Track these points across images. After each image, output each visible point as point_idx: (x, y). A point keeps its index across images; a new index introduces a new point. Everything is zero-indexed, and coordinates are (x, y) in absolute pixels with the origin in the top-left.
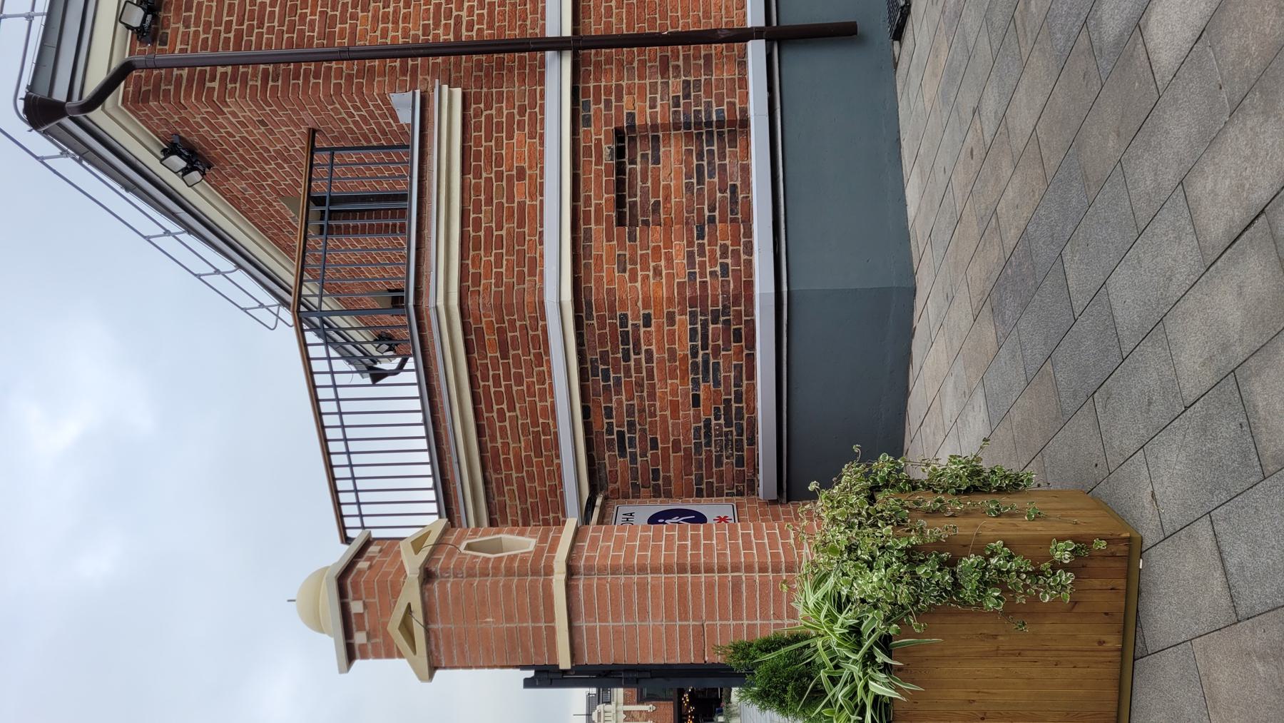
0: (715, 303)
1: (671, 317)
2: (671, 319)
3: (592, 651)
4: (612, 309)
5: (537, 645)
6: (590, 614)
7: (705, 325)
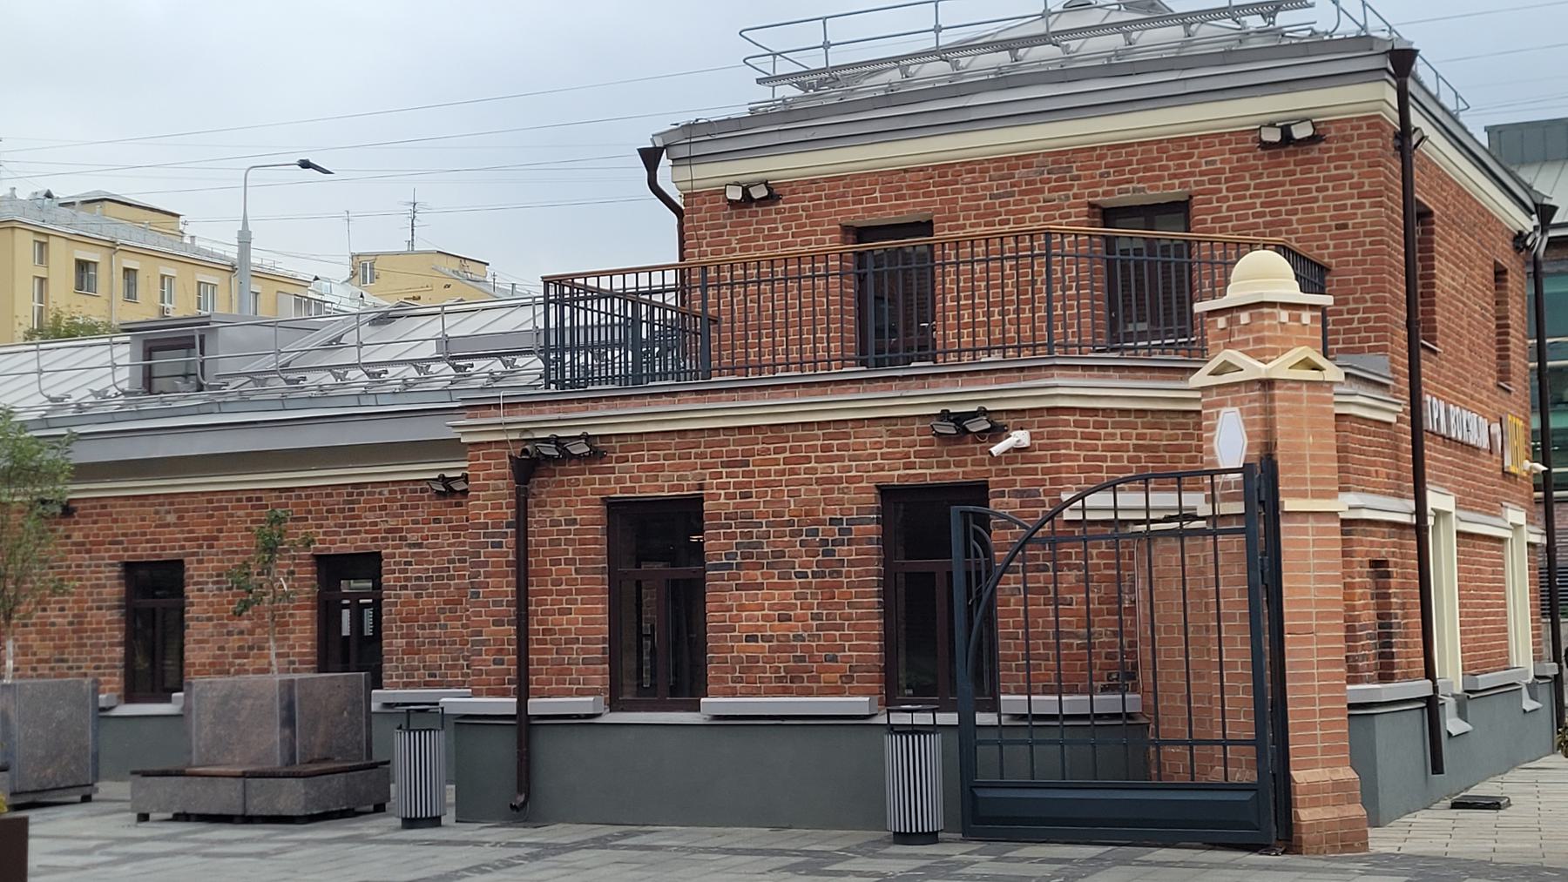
5: (1293, 481)
6: (1319, 531)
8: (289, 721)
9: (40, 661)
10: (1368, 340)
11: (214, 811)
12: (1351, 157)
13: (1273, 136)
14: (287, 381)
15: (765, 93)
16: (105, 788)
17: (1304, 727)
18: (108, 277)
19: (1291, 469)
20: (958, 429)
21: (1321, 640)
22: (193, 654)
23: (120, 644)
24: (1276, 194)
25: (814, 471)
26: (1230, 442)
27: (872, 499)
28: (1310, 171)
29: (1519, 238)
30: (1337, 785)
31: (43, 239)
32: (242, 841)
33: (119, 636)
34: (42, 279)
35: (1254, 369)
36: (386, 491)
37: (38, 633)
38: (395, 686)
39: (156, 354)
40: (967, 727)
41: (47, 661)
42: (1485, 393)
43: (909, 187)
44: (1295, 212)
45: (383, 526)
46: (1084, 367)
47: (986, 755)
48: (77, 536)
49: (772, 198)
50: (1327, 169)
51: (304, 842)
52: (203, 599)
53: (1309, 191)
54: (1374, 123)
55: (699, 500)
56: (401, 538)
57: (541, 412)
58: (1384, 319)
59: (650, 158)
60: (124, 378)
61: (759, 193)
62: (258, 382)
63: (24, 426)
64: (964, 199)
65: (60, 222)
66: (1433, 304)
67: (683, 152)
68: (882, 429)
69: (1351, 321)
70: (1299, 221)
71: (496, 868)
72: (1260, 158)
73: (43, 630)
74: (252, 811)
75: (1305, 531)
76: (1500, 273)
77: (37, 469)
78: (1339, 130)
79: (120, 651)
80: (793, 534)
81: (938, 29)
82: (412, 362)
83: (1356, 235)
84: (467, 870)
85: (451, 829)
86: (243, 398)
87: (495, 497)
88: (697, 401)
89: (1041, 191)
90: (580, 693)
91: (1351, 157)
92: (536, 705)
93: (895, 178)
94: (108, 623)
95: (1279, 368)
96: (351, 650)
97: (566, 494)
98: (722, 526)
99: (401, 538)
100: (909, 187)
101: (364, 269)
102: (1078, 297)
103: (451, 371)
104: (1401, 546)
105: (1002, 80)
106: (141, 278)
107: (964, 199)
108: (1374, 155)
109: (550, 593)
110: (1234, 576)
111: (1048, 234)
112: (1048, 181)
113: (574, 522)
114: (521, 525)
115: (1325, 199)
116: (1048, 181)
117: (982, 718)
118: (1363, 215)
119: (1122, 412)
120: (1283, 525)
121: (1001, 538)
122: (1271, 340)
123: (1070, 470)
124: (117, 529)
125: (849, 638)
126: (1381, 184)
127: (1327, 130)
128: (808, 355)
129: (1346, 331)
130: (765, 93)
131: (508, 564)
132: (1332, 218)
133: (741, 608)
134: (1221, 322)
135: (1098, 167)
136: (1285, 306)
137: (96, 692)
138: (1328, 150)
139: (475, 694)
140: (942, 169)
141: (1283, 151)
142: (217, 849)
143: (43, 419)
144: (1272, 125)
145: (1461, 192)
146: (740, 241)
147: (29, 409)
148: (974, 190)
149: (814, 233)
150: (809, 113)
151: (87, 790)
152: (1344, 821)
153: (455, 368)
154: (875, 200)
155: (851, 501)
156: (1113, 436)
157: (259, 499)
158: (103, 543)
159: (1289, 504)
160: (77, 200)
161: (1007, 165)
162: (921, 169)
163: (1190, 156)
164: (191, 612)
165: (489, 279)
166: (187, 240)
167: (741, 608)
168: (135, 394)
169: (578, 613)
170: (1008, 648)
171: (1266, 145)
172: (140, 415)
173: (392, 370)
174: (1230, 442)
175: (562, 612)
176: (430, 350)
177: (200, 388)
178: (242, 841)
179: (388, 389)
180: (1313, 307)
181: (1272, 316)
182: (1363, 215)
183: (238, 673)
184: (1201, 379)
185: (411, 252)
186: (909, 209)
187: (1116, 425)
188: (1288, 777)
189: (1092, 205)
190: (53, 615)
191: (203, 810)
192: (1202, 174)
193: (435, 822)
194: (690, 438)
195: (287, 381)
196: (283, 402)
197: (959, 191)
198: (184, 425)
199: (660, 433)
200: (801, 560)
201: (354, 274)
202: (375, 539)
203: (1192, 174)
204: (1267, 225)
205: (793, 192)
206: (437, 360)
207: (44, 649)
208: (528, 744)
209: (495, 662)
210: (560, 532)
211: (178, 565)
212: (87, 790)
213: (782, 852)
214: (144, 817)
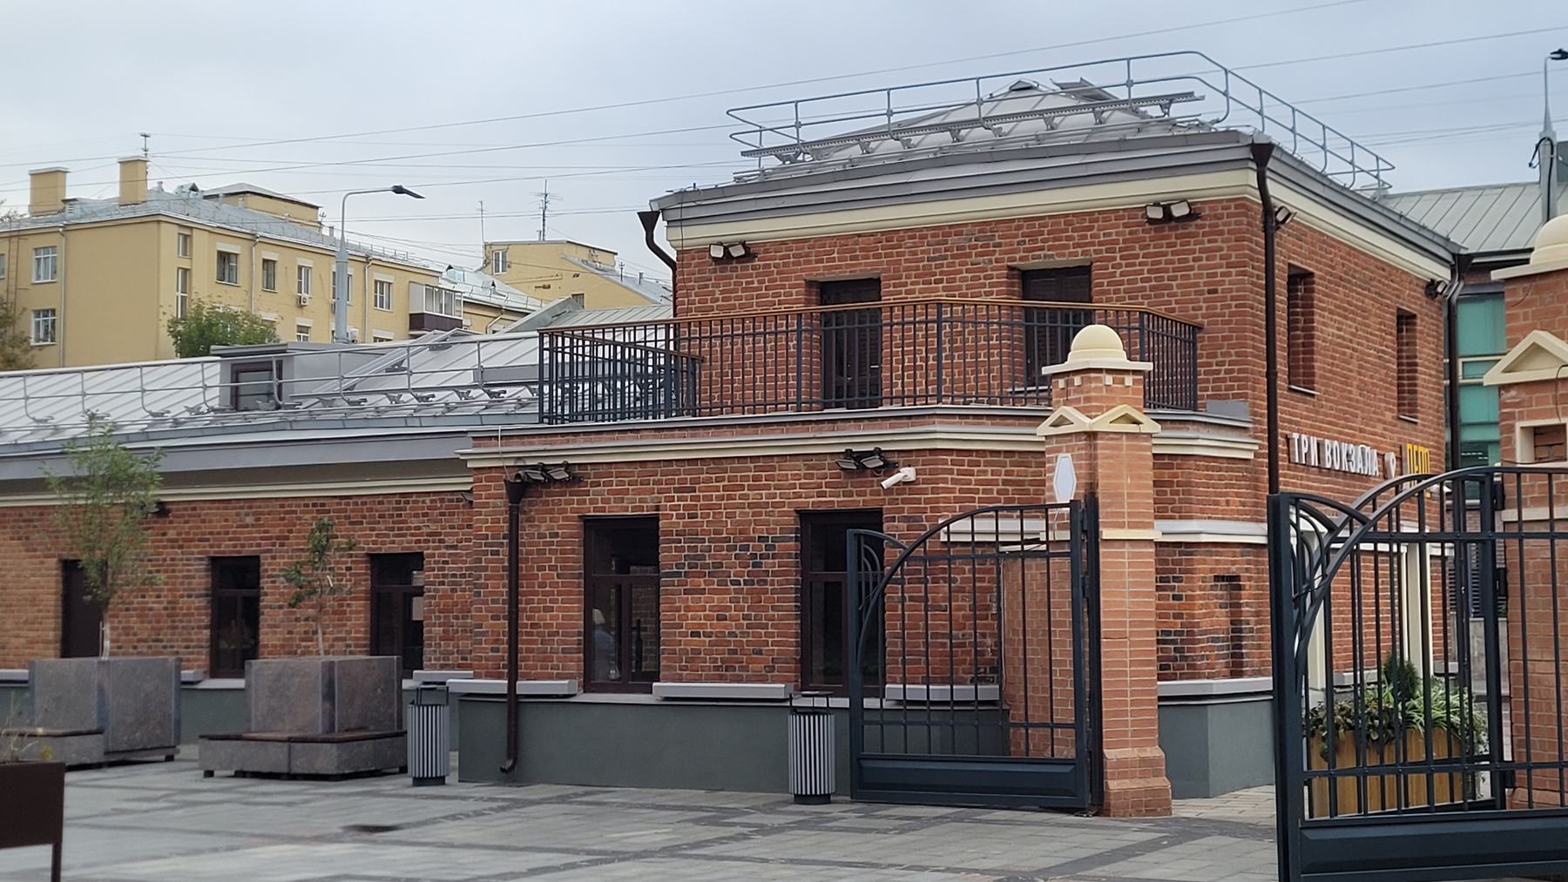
0: (1190, 650)
1: (1179, 616)
2: (1178, 616)
3: (1108, 555)
4: (1187, 571)
5: (1112, 514)
6: (1133, 555)
7: (1173, 642)
8: (329, 696)
9: (139, 641)
10: (1232, 388)
11: (265, 769)
12: (1221, 233)
13: (1157, 214)
14: (350, 403)
15: (751, 164)
16: (187, 750)
17: (1116, 714)
18: (248, 269)
19: (1110, 505)
20: (858, 465)
21: (1133, 644)
22: (267, 637)
23: (206, 627)
24: (1159, 263)
25: (746, 497)
26: (1064, 484)
27: (791, 521)
28: (1188, 243)
29: (1431, 287)
30: (1144, 761)
31: (187, 232)
32: (279, 793)
33: (206, 620)
34: (185, 271)
35: (1082, 422)
36: (428, 500)
37: (139, 616)
38: (433, 667)
39: (242, 375)
40: (856, 710)
41: (145, 641)
42: (1380, 426)
43: (862, 250)
44: (1174, 278)
45: (425, 530)
46: (960, 416)
47: (871, 733)
48: (172, 534)
49: (749, 255)
50: (1202, 242)
51: (327, 795)
52: (273, 591)
53: (1186, 260)
54: (1241, 204)
55: (656, 519)
56: (441, 541)
57: (532, 444)
58: (1245, 371)
59: (648, 220)
60: (215, 397)
61: (738, 252)
62: (325, 403)
63: (129, 438)
64: (907, 261)
65: (205, 214)
66: (1312, 352)
67: (676, 215)
68: (801, 463)
69: (1218, 372)
70: (1178, 286)
71: (468, 816)
72: (1148, 232)
73: (143, 613)
74: (295, 770)
75: (1122, 555)
76: (1405, 320)
77: (132, 477)
78: (1211, 209)
79: (206, 633)
80: (729, 549)
81: (890, 113)
82: (455, 388)
83: (1224, 299)
84: (445, 818)
85: (453, 786)
86: (312, 416)
87: (495, 513)
88: (655, 437)
89: (970, 255)
90: (559, 677)
91: (1221, 233)
92: (523, 687)
93: (851, 241)
94: (197, 608)
95: (1101, 423)
96: (396, 632)
97: (551, 512)
98: (674, 541)
99: (441, 541)
100: (862, 250)
101: (497, 258)
102: (1000, 346)
103: (486, 397)
104: (1257, 563)
105: (942, 159)
106: (279, 269)
107: (907, 261)
108: (1240, 231)
109: (536, 594)
110: (1062, 590)
111: (940, 305)
112: (975, 247)
113: (557, 535)
114: (513, 537)
115: (1200, 268)
116: (975, 247)
117: (869, 703)
118: (1230, 282)
119: (993, 452)
120: (1102, 550)
121: (891, 555)
122: (1096, 399)
123: (947, 500)
124: (205, 528)
125: (772, 635)
126: (1245, 256)
127: (1202, 209)
128: (760, 399)
129: (1215, 381)
130: (751, 164)
131: (504, 569)
132: (1205, 284)
133: (688, 609)
134: (1061, 383)
135: (1016, 236)
136: (1109, 371)
137: (179, 668)
138: (1203, 226)
139: (476, 676)
140: (889, 234)
141: (1166, 226)
142: (258, 799)
143: (143, 432)
144: (1157, 204)
145: (1352, 252)
146: (722, 292)
147: (133, 423)
148: (915, 253)
149: (783, 287)
150: (781, 184)
151: (170, 751)
152: (1148, 791)
153: (490, 394)
154: (833, 260)
155: (776, 523)
156: (985, 472)
157: (323, 505)
158: (192, 540)
159: (1106, 533)
160: (220, 193)
161: (942, 232)
162: (872, 235)
163: (1091, 228)
164: (265, 601)
165: (617, 269)
166: (326, 232)
167: (688, 609)
168: (223, 411)
169: (559, 610)
170: (893, 646)
171: (1152, 221)
172: (224, 431)
173: (439, 395)
174: (1064, 484)
175: (546, 610)
176: (468, 379)
177: (279, 407)
178: (279, 793)
179: (432, 412)
180: (1135, 372)
181: (1098, 380)
182: (1230, 282)
183: (303, 654)
184: (1044, 429)
185: (542, 242)
186: (861, 269)
187: (987, 464)
188: (1101, 755)
189: (1010, 268)
190: (150, 601)
191: (256, 769)
192: (1101, 244)
193: (440, 781)
194: (649, 468)
195: (350, 403)
196: (344, 423)
197: (902, 254)
198: (264, 439)
199: (632, 460)
200: (735, 570)
201: (486, 263)
202: (418, 541)
203: (1092, 244)
204: (1152, 288)
205: (766, 251)
206: (475, 387)
207: (143, 630)
208: (516, 719)
209: (493, 650)
210: (545, 544)
211: (255, 560)
212: (170, 751)
213: (700, 809)
214: (209, 774)
